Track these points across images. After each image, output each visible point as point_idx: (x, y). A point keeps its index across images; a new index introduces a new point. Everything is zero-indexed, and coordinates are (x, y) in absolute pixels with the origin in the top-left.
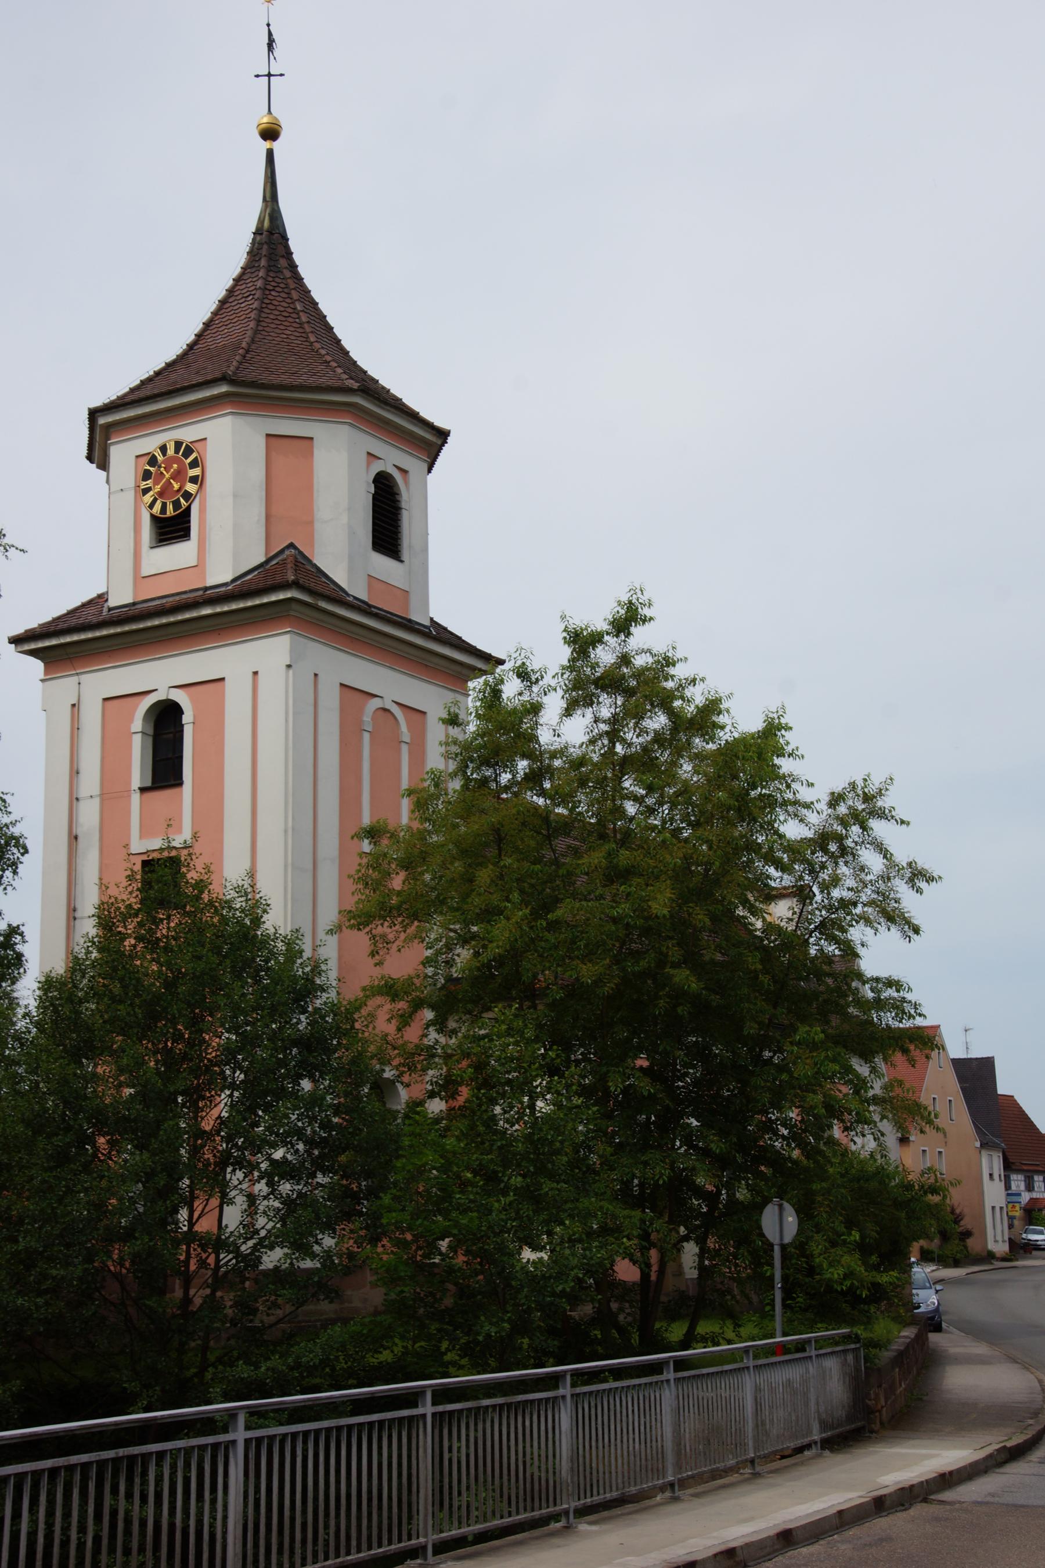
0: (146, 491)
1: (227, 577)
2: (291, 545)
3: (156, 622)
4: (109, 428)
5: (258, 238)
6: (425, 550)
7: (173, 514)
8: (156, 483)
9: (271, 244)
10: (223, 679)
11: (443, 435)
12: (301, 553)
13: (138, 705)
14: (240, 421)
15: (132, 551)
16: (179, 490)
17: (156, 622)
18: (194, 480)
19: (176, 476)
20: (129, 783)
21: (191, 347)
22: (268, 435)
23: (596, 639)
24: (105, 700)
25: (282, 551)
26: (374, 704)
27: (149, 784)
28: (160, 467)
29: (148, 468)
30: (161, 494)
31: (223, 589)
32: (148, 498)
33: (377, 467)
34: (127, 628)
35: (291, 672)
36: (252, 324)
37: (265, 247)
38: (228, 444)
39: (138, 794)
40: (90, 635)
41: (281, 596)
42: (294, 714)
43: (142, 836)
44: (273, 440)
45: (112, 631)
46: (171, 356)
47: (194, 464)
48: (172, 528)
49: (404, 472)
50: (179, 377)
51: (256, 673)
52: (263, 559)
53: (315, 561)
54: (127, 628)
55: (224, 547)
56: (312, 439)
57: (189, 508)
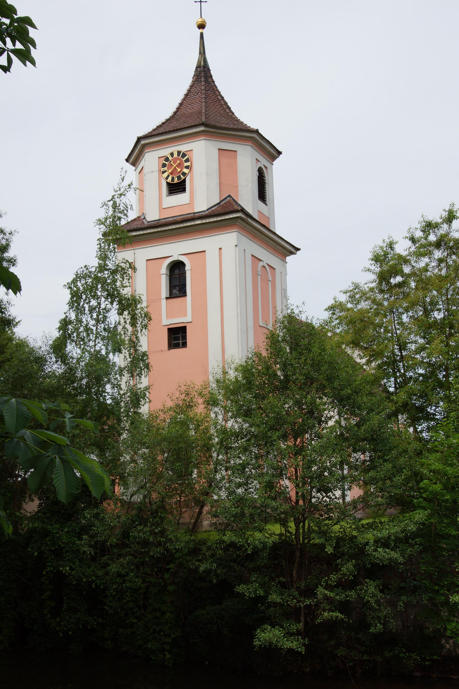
0: (163, 172)
1: (205, 209)
2: (229, 196)
3: (174, 227)
4: (144, 146)
5: (199, 69)
6: (273, 201)
7: (170, 182)
8: (168, 169)
9: (203, 73)
10: (205, 251)
11: (280, 153)
12: (233, 199)
13: (163, 263)
14: (208, 143)
15: (158, 197)
16: (180, 172)
17: (174, 227)
18: (187, 167)
19: (179, 165)
20: (160, 295)
21: (175, 113)
22: (219, 149)
23: (436, 226)
24: (147, 260)
25: (226, 198)
26: (261, 264)
27: (168, 296)
28: (171, 162)
29: (165, 162)
30: (171, 173)
31: (203, 213)
32: (166, 175)
33: (259, 165)
34: (159, 229)
35: (237, 248)
36: (204, 104)
37: (203, 73)
38: (202, 152)
39: (165, 300)
40: (141, 232)
41: (235, 215)
42: (239, 266)
43: (168, 317)
44: (221, 151)
45: (152, 231)
46: (168, 117)
47: (187, 161)
48: (177, 187)
49: (266, 168)
50: (175, 125)
51: (220, 249)
52: (219, 201)
53: (239, 203)
54: (159, 229)
55: (201, 196)
56: (236, 151)
57: (185, 179)
